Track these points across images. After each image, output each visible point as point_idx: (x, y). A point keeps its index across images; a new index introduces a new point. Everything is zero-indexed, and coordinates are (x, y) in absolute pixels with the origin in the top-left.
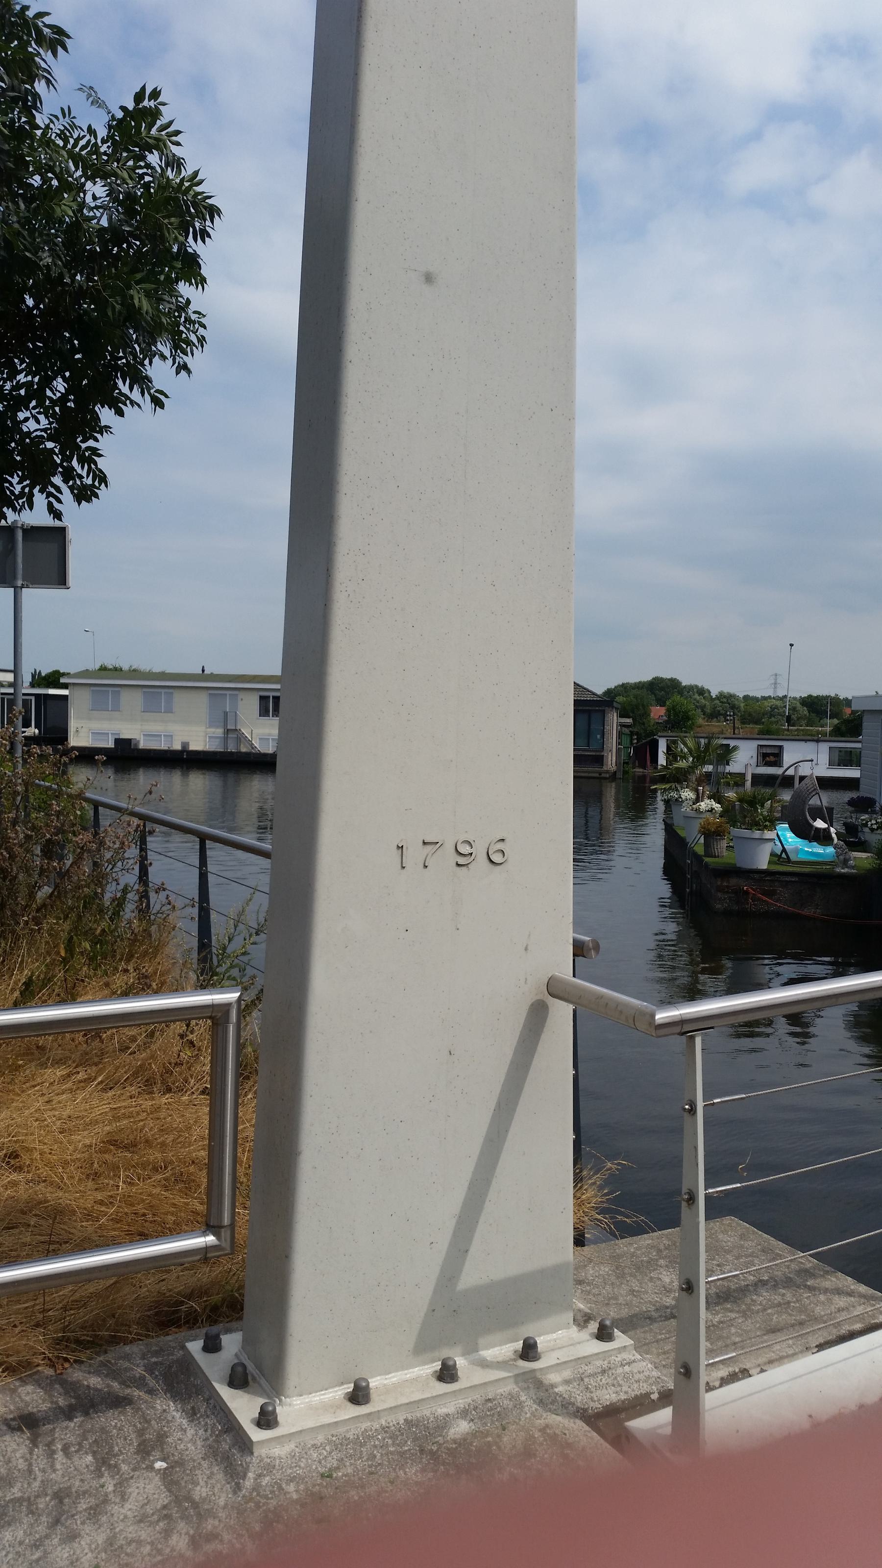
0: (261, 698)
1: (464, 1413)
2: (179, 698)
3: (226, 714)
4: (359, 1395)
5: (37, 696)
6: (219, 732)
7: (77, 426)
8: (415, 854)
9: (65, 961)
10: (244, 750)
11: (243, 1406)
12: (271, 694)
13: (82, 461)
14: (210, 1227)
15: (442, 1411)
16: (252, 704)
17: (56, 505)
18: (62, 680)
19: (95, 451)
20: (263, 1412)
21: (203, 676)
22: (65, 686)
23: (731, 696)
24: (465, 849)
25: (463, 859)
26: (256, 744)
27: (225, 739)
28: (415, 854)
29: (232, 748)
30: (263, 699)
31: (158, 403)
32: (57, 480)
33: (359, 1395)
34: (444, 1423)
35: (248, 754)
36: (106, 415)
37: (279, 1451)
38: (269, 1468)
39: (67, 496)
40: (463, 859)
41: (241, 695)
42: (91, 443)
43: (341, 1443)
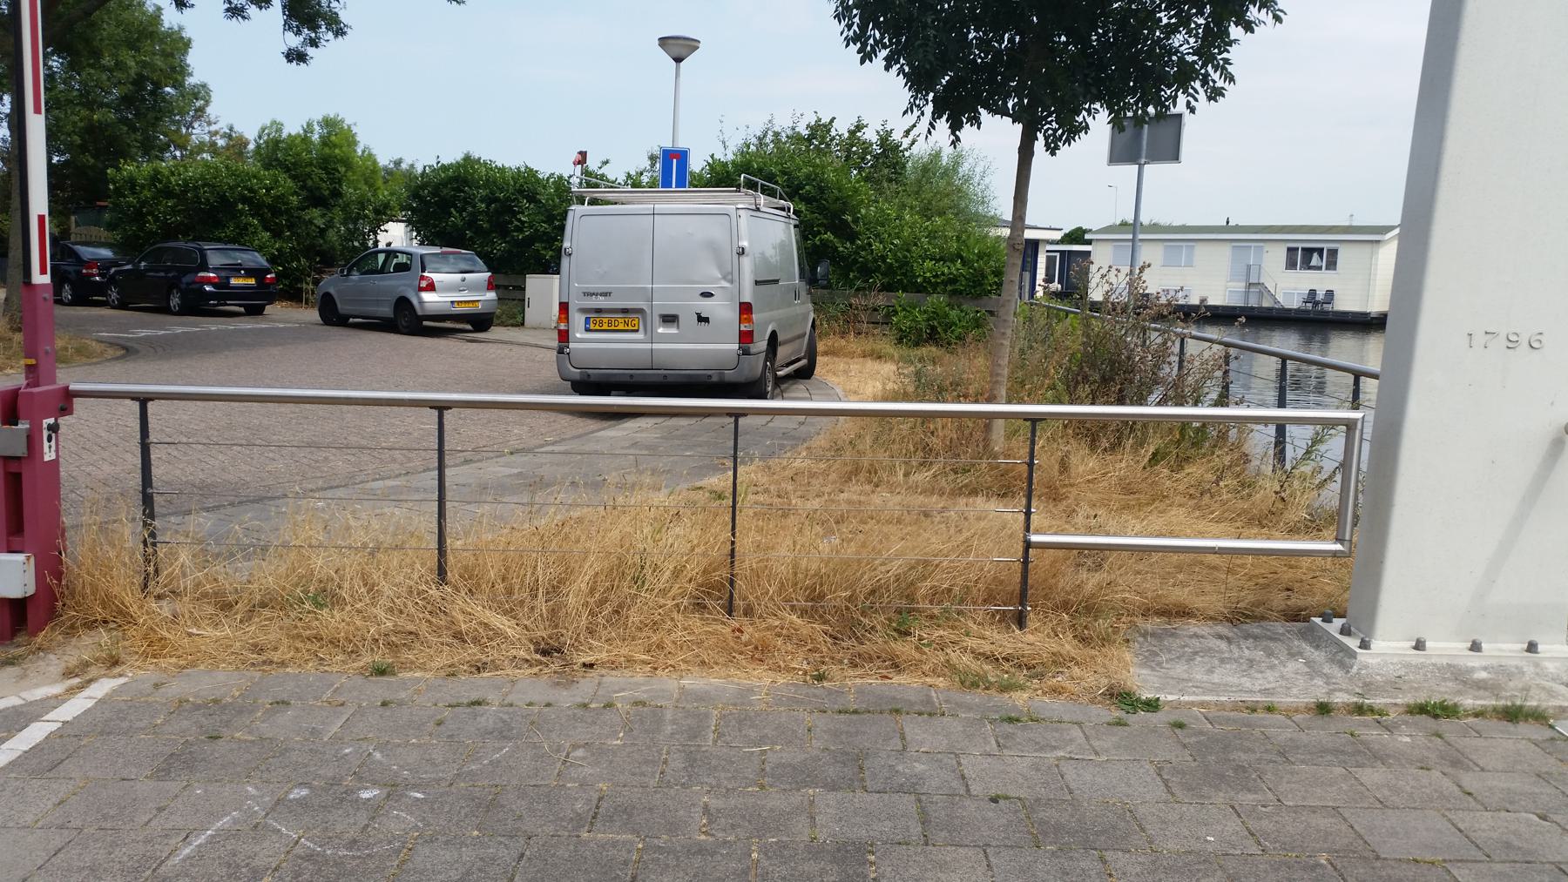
0: (1289, 249)
1: (1485, 669)
2: (1201, 252)
3: (1249, 267)
4: (1419, 646)
5: (1062, 253)
6: (1240, 286)
7: (1214, 42)
8: (1480, 339)
9: (1179, 442)
10: (1266, 304)
11: (1352, 643)
12: (1300, 245)
13: (1216, 69)
14: (1338, 540)
15: (1470, 664)
16: (1280, 254)
17: (1193, 103)
18: (1087, 237)
19: (1227, 61)
20: (1363, 641)
21: (1227, 228)
22: (1089, 242)
23: (532, 173)
24: (1513, 338)
25: (1512, 344)
26: (1280, 298)
27: (1247, 293)
28: (1480, 339)
29: (1253, 303)
30: (1292, 251)
31: (1277, 19)
32: (1197, 84)
33: (1419, 646)
34: (1472, 670)
35: (1270, 309)
36: (1235, 31)
37: (1372, 661)
38: (1366, 667)
39: (1202, 96)
40: (1512, 344)
41: (1267, 247)
42: (1225, 55)
43: (1407, 666)
